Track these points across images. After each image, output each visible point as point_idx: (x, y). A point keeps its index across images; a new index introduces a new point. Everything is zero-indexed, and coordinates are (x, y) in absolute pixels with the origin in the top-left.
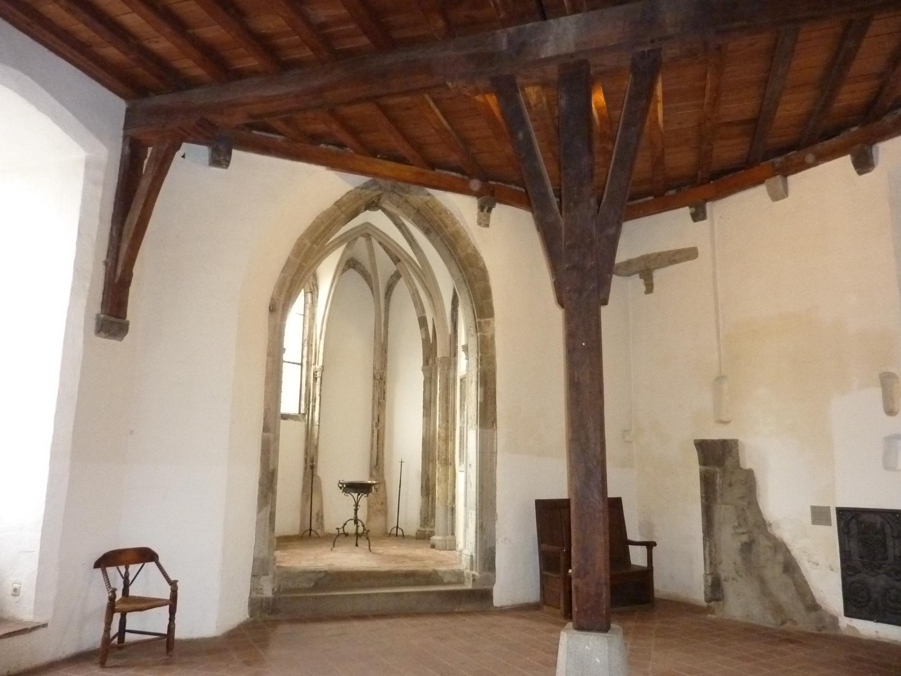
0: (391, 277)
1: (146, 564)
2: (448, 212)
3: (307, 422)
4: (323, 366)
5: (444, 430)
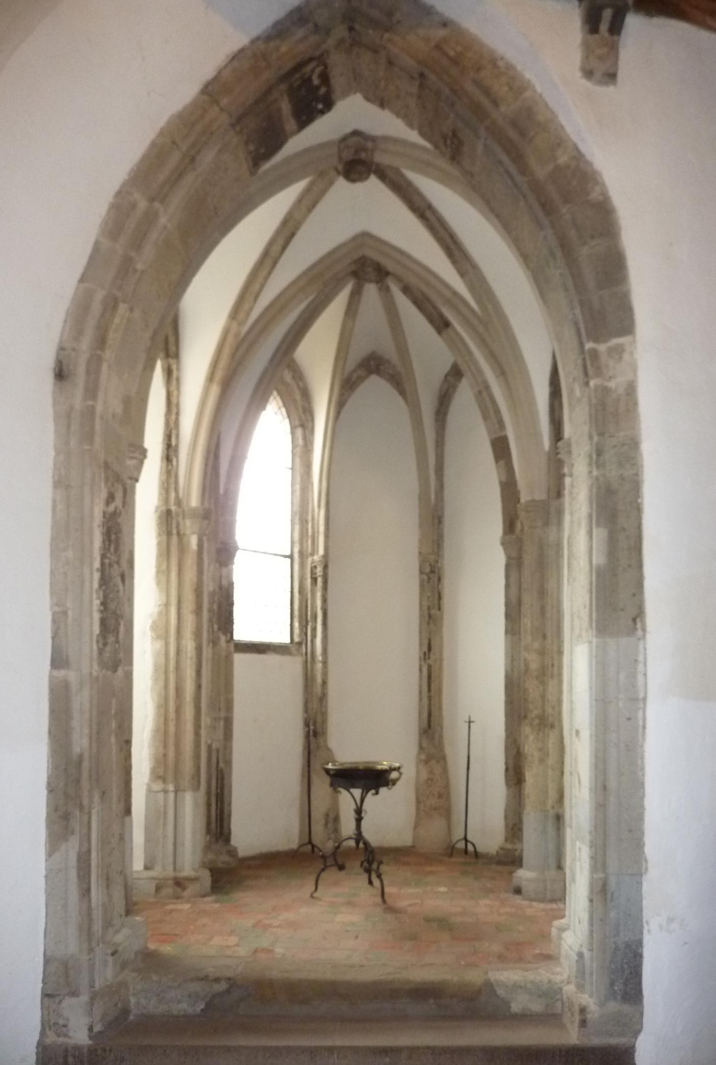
0: (446, 376)
2: (501, 64)
3: (304, 657)
4: (326, 556)
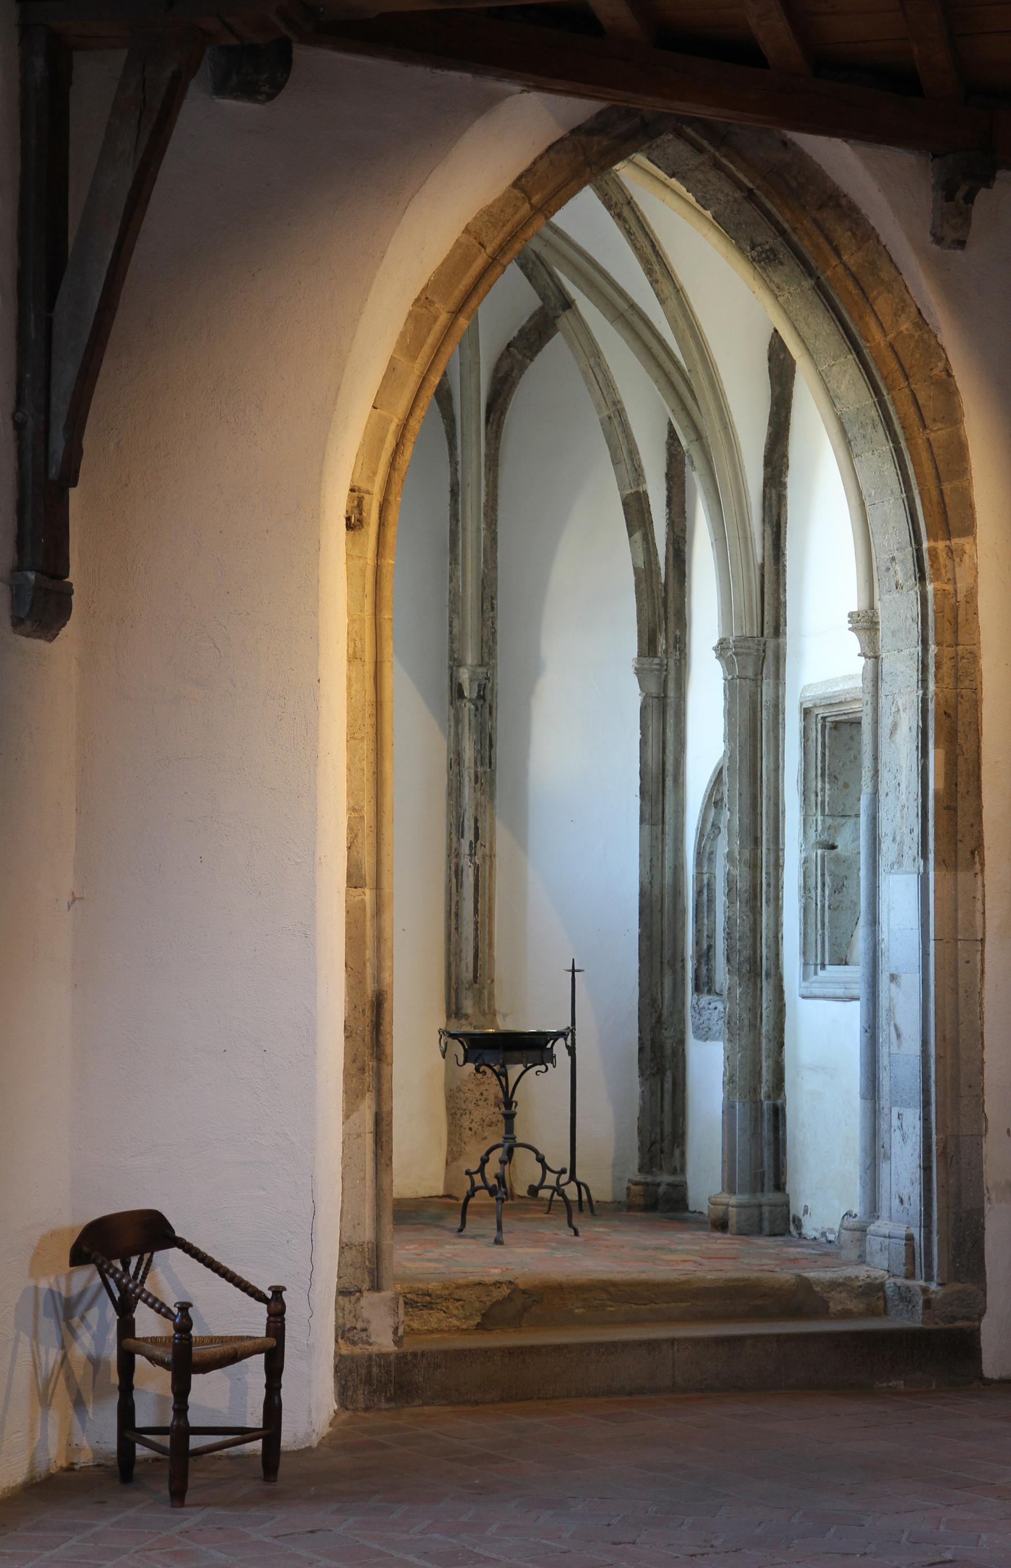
0: (509, 346)
1: (156, 1254)
2: (843, 202)
5: (746, 870)
